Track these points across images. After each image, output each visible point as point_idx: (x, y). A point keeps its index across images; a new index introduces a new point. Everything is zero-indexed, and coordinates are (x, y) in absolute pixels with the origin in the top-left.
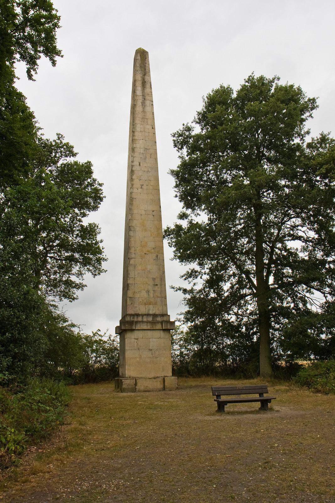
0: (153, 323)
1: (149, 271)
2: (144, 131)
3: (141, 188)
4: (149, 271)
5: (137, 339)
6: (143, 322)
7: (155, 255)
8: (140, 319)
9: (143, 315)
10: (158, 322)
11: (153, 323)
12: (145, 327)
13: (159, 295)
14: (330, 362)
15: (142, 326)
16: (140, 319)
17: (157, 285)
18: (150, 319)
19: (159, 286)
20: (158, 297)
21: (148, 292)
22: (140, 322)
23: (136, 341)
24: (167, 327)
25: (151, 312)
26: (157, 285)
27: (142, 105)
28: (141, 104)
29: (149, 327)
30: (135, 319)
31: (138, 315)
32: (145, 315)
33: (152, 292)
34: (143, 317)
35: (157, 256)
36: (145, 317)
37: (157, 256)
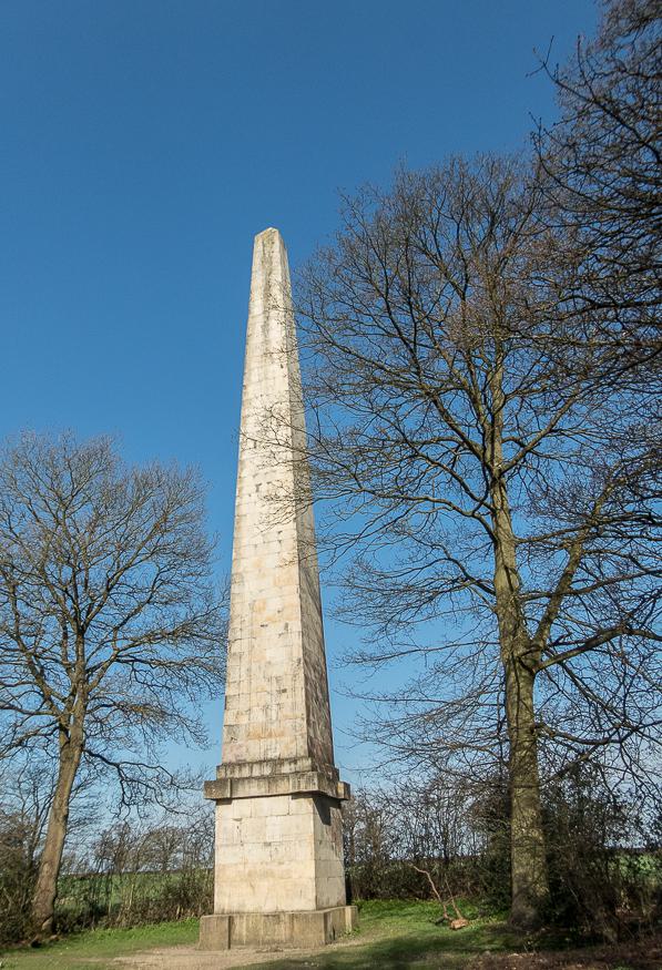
0: (271, 779)
1: (269, 663)
2: (266, 378)
3: (257, 491)
4: (269, 663)
5: (240, 820)
6: (249, 778)
7: (282, 625)
8: (246, 772)
9: (251, 764)
10: (286, 776)
11: (271, 779)
12: (254, 791)
13: (290, 714)
14: (5, 694)
15: (247, 789)
16: (246, 772)
17: (285, 691)
18: (267, 771)
19: (289, 692)
20: (286, 717)
21: (266, 708)
22: (244, 779)
23: (237, 823)
24: (299, 786)
25: (271, 755)
26: (285, 691)
27: (263, 331)
28: (260, 330)
29: (263, 791)
31: (241, 764)
32: (256, 763)
33: (275, 707)
34: (252, 768)
35: (287, 626)
36: (256, 767)
37: (287, 626)
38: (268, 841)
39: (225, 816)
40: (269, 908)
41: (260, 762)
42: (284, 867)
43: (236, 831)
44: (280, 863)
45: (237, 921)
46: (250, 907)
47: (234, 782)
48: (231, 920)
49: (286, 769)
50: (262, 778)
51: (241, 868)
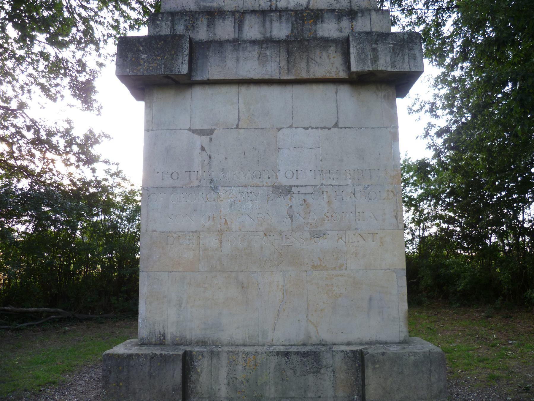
6: (237, 43)
8: (225, 30)
12: (250, 66)
15: (230, 63)
16: (225, 30)
23: (200, 140)
24: (375, 60)
29: (273, 68)
30: (202, 34)
32: (253, 12)
38: (284, 181)
39: (132, 18)
40: (287, 331)
41: (263, 14)
42: (324, 244)
43: (198, 158)
44: (317, 234)
45: (203, 365)
46: (234, 327)
47: (197, 50)
48: (187, 362)
49: (329, 29)
50: (267, 42)
51: (212, 241)
